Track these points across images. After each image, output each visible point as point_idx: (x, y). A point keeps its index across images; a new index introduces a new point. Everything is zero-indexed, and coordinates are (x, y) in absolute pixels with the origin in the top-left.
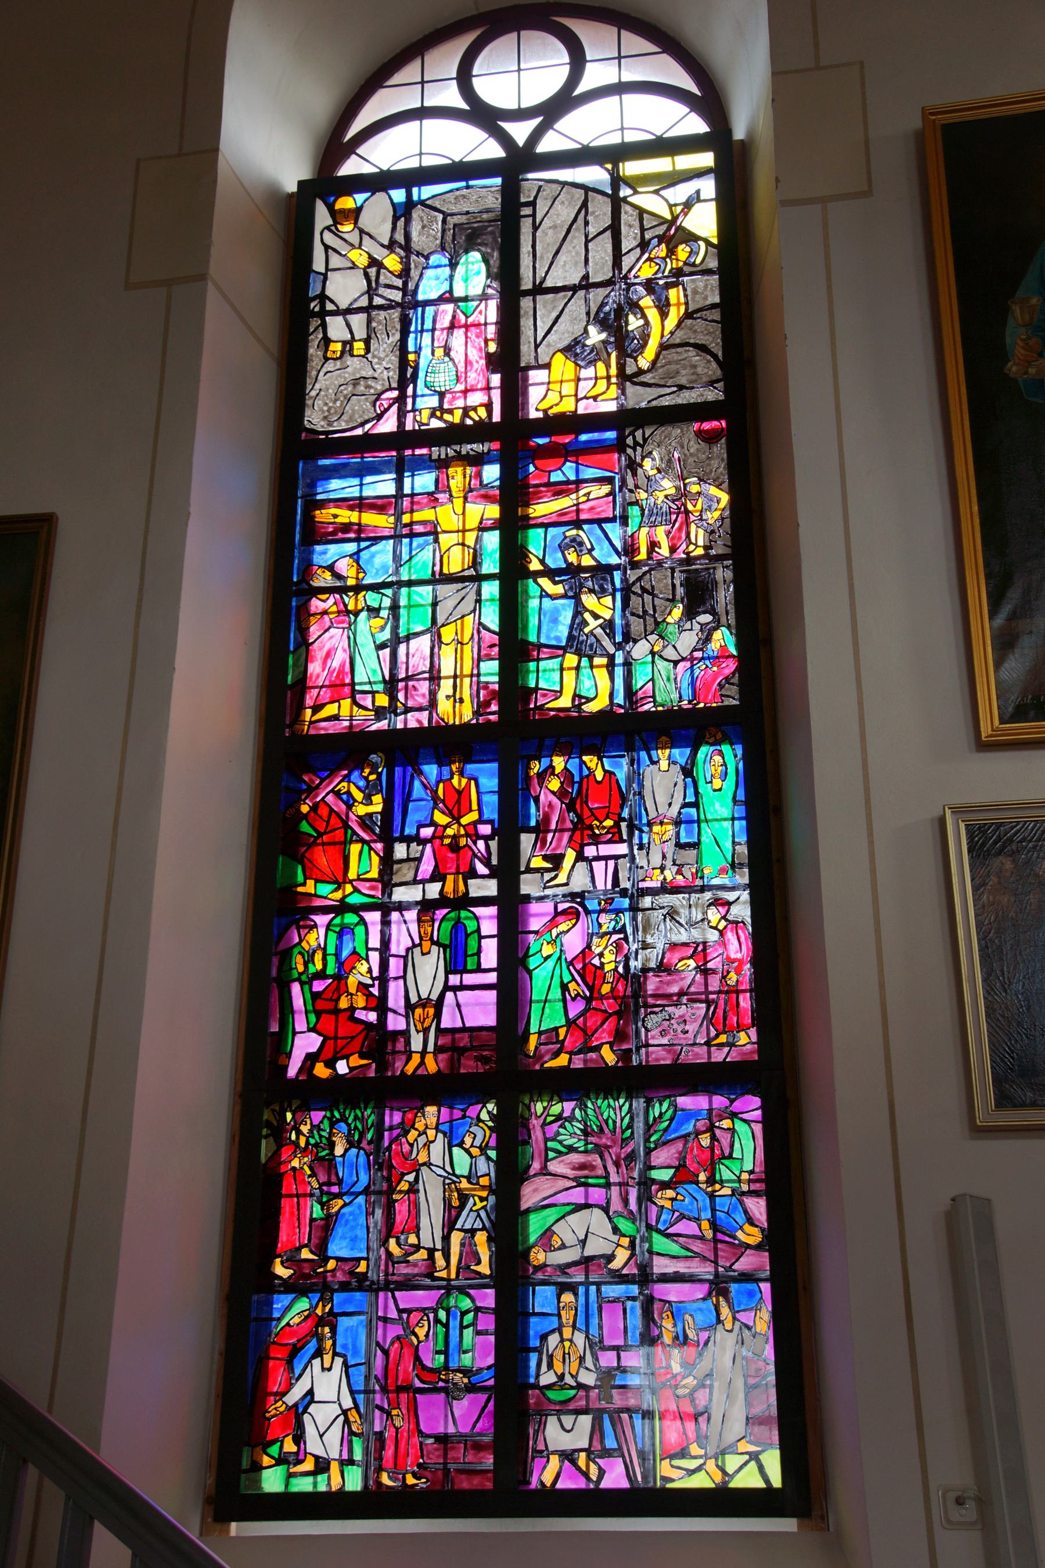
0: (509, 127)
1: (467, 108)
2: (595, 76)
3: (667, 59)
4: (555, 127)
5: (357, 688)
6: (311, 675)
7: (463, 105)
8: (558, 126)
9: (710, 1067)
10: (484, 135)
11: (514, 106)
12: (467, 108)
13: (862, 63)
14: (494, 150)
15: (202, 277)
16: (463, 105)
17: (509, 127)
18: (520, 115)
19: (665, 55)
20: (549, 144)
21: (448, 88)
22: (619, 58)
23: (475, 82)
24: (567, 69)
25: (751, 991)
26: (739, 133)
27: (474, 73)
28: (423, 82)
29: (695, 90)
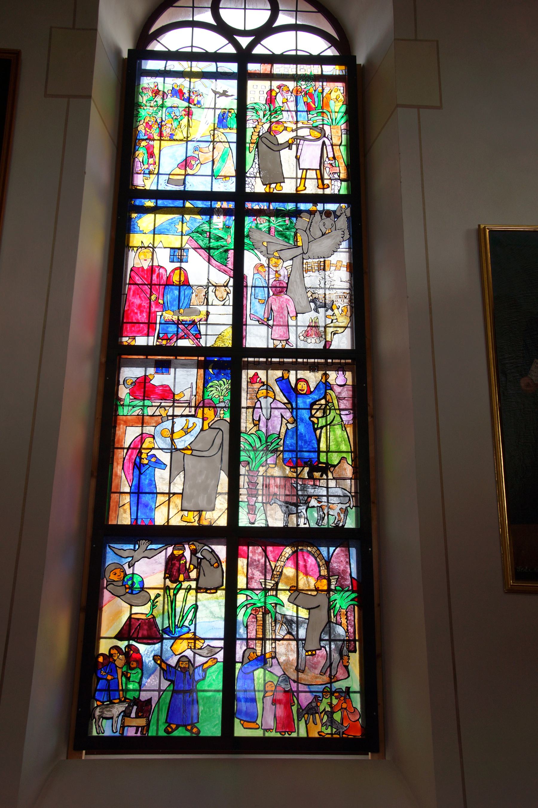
0: (240, 39)
1: (215, 24)
2: (283, 19)
3: (320, 16)
4: (262, 42)
5: (170, 451)
6: (145, 663)
7: (213, 22)
8: (263, 42)
9: (238, 129)
10: (227, 42)
11: (242, 28)
12: (215, 24)
13: (437, 42)
14: (230, 49)
15: (90, 97)
16: (213, 22)
17: (240, 39)
18: (245, 33)
19: (319, 14)
20: (258, 50)
21: (207, 11)
22: (296, 11)
23: (221, 11)
24: (268, 13)
25: (248, 108)
26: (361, 60)
27: (221, 6)
28: (193, 7)
29: (335, 36)
